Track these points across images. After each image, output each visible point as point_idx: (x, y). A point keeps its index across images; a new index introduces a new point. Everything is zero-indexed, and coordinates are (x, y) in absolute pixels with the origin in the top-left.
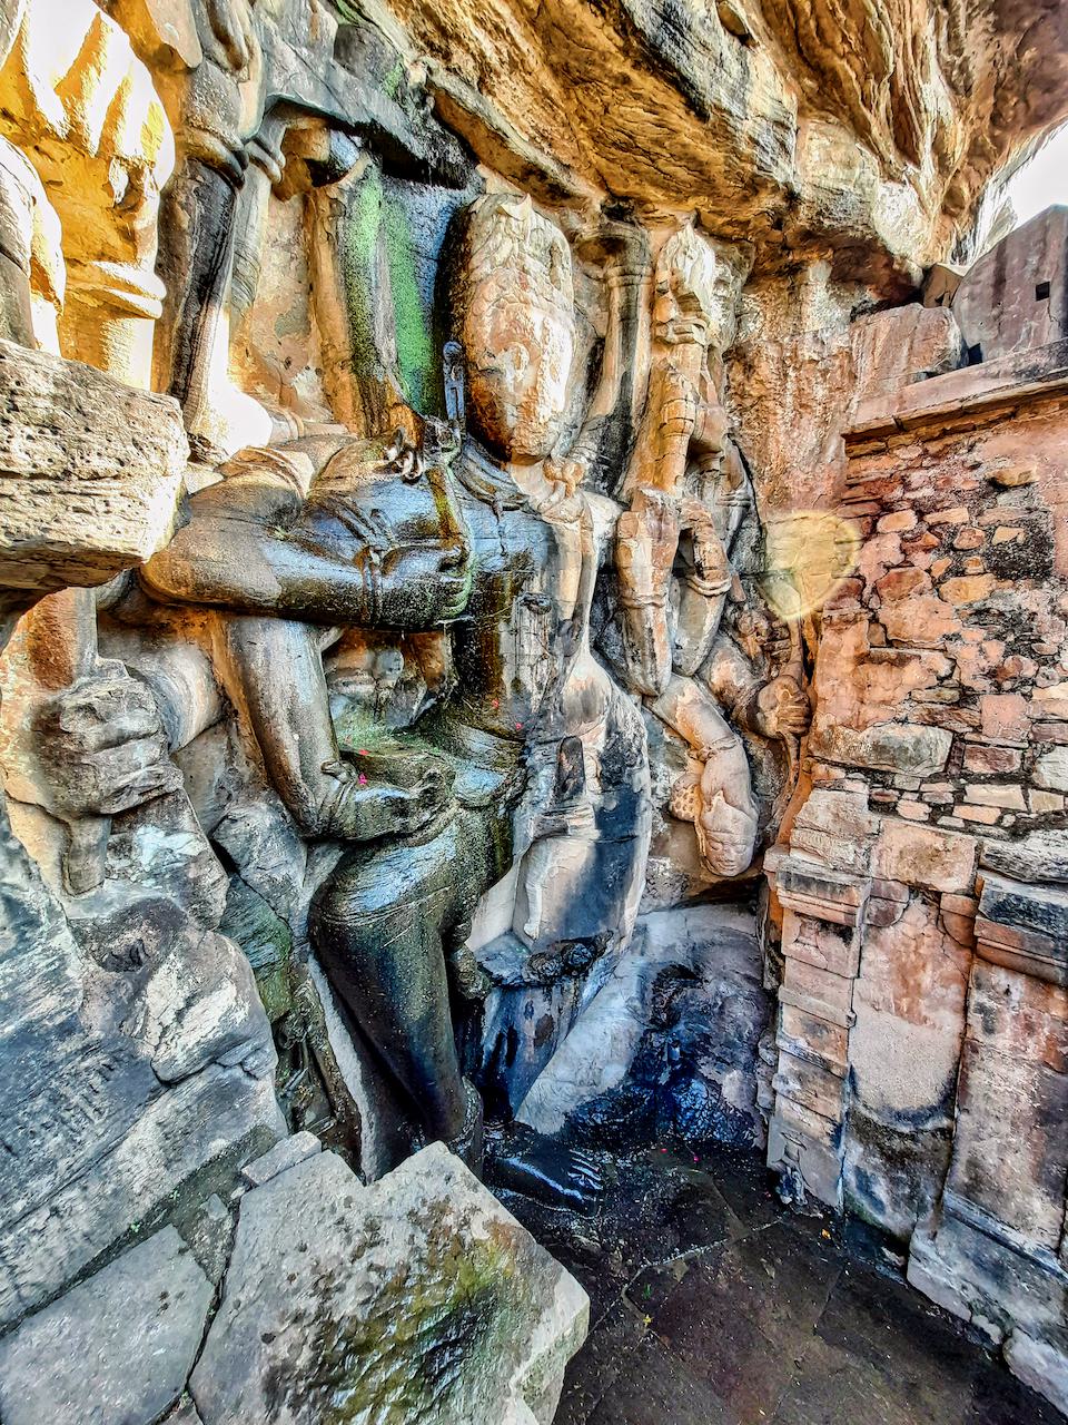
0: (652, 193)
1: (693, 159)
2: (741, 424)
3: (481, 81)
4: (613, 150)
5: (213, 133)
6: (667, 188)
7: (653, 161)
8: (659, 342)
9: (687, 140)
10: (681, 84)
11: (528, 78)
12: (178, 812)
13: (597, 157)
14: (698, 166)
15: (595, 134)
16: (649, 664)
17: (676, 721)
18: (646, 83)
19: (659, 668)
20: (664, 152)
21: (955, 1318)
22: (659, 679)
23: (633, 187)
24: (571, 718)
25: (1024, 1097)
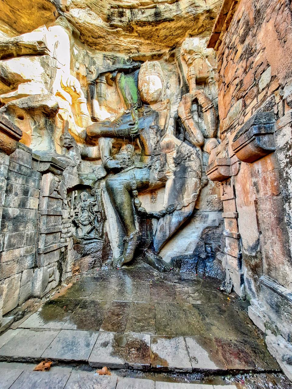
0: (177, 40)
1: (178, 28)
3: (138, 51)
6: (179, 37)
9: (174, 26)
10: (165, 20)
14: (182, 27)
18: (160, 26)
19: (195, 136)
20: (173, 32)
21: (259, 330)
22: (197, 139)
23: (173, 42)
24: (163, 149)
25: (272, 215)
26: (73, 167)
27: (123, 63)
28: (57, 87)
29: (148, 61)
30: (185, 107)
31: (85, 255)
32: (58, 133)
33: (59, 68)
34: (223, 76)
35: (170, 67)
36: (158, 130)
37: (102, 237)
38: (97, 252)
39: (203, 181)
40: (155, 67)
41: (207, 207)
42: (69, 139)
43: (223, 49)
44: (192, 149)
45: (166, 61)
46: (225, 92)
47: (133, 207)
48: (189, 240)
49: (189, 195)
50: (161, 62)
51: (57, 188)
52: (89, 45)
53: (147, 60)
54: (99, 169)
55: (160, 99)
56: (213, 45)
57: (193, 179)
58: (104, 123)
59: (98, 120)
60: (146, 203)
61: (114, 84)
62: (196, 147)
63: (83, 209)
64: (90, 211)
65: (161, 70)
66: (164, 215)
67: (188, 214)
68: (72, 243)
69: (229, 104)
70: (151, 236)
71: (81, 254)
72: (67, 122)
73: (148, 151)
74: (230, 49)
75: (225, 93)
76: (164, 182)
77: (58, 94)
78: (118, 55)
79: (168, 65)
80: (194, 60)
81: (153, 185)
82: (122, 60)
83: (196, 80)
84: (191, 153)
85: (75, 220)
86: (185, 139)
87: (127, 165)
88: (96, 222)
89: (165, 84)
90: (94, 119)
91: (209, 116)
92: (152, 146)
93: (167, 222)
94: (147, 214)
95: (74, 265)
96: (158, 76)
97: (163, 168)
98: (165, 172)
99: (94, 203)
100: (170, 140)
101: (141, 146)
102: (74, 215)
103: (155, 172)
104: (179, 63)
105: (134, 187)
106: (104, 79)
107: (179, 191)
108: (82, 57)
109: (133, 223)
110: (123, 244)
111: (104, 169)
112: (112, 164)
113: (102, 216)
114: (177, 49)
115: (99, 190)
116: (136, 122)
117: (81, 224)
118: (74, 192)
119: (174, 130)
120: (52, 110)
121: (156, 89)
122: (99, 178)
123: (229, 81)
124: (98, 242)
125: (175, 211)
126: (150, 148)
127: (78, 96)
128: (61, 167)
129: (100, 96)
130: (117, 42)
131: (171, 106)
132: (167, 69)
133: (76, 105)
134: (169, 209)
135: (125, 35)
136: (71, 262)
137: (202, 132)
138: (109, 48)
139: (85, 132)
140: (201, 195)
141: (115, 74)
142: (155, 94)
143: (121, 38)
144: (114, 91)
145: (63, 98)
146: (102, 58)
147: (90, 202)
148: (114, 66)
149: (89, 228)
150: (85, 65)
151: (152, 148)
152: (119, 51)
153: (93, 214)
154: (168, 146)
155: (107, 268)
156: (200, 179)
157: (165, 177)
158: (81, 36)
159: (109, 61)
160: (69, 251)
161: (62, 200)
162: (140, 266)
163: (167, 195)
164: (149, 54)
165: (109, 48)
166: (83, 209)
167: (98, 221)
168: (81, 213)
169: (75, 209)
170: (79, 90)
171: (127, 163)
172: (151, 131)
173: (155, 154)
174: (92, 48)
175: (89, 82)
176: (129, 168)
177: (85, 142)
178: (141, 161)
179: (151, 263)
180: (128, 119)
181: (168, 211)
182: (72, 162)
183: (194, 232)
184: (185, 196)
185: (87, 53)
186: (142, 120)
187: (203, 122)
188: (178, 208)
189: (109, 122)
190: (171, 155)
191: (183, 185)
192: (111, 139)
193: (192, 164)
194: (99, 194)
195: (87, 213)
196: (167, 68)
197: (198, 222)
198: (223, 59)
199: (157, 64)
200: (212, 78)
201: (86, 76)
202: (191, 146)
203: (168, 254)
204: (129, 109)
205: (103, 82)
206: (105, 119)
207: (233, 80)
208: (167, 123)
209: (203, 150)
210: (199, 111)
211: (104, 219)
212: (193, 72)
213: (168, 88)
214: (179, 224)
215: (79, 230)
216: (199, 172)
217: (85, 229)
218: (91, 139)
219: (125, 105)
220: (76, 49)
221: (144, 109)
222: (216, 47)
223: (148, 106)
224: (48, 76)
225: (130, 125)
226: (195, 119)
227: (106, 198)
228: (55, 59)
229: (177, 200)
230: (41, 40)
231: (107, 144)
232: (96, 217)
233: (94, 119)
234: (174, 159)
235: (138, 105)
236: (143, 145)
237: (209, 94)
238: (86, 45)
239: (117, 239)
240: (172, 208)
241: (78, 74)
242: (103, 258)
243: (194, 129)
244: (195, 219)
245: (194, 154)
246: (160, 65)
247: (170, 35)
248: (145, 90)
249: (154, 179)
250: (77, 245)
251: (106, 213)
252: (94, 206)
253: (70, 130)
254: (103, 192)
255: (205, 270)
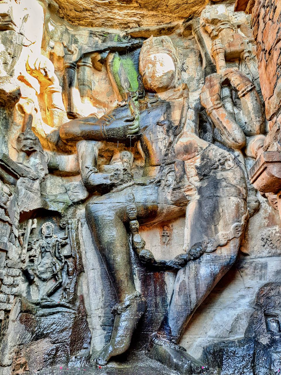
0: (194, 9)
4: (176, 10)
5: (67, 63)
7: (187, 3)
11: (147, 16)
12: (37, 155)
13: (175, 15)
15: (170, 12)
16: (226, 133)
19: (230, 132)
23: (189, 12)
24: (178, 154)
26: (34, 180)
27: (118, 41)
28: (19, 68)
29: (154, 36)
30: (211, 93)
31: (39, 337)
32: (15, 132)
33: (26, 46)
34: (261, 42)
35: (186, 43)
36: (170, 127)
37: (73, 302)
38: (62, 331)
39: (250, 204)
40: (164, 43)
41: (263, 249)
42: (31, 139)
43: (257, 10)
44: (226, 153)
45: (180, 35)
46: (267, 61)
47: (132, 250)
48: (234, 312)
49: (226, 225)
50: (173, 37)
51: (5, 204)
52: (70, 20)
53: (152, 36)
54: (75, 187)
55: (172, 85)
56: (243, 7)
57: (233, 198)
58: (86, 120)
59: (78, 116)
60: (154, 244)
61: (103, 69)
62: (233, 151)
63: (43, 251)
64: (55, 256)
65: (172, 46)
66: (184, 263)
67: (228, 260)
68: (19, 308)
69: (274, 76)
70: (163, 306)
71: (33, 334)
72: (31, 117)
73: (155, 160)
74: (267, 7)
75: (267, 63)
76: (183, 208)
77: (21, 79)
78: (110, 31)
79: (183, 40)
80: (220, 30)
81: (165, 211)
82: (116, 37)
83: (226, 57)
84: (225, 158)
85: (29, 268)
86: (214, 140)
87: (122, 181)
88: (64, 275)
89: (179, 65)
90: (71, 115)
91: (249, 102)
92: (161, 151)
93: (192, 275)
94: (155, 262)
95: (18, 353)
96: (169, 54)
97: (180, 184)
98: (183, 190)
99: (64, 241)
100: (189, 141)
101: (144, 152)
102: (27, 260)
103: (166, 190)
104: (198, 37)
105: (133, 214)
106: (89, 61)
107: (209, 217)
108: (59, 34)
109: (131, 278)
110: (111, 324)
111: (84, 187)
112: (97, 179)
113: (76, 265)
114: (194, 20)
115: (74, 221)
116: (136, 117)
117: (38, 276)
118: (31, 221)
119: (195, 126)
120: (10, 97)
121: (166, 72)
122: (76, 200)
123: (270, 47)
124: (66, 312)
125: (205, 254)
126: (158, 154)
127: (50, 82)
128: (15, 171)
129: (82, 84)
130: (109, 15)
131: (190, 93)
132: (181, 46)
133: (46, 96)
134: (193, 251)
135: (120, 6)
136: (13, 345)
137: (241, 127)
138: (97, 23)
139: (56, 133)
140: (250, 228)
141: (105, 55)
142: (165, 77)
143: (116, 10)
144: (104, 77)
145: (28, 84)
146: (88, 35)
147: (56, 239)
148: (105, 44)
149: (51, 285)
150: (62, 43)
151: (161, 154)
152: (112, 26)
153: (61, 261)
154: (188, 150)
155: (78, 365)
156: (245, 200)
157: (184, 197)
158: (60, 10)
159: (97, 39)
160: (10, 322)
161: (11, 225)
162: (141, 364)
163: (189, 229)
164: (155, 28)
165: (97, 22)
166: (43, 251)
167: (68, 274)
168: (40, 257)
169: (29, 250)
170: (51, 74)
171: (121, 177)
172: (158, 129)
173: (167, 162)
174: (74, 23)
175: (67, 64)
176: (125, 185)
177: (55, 148)
178: (145, 175)
179: (163, 359)
180: (124, 114)
181: (192, 255)
182: (33, 172)
183: (243, 297)
184: (220, 227)
185: (67, 30)
186: (145, 114)
187: (241, 112)
188: (209, 249)
189: (94, 119)
190: (192, 163)
191: (215, 209)
192: (97, 142)
193: (229, 175)
194: (73, 226)
195: (51, 258)
196: (182, 44)
197: (249, 277)
198: (258, 22)
199: (166, 40)
200: (249, 52)
201: (63, 57)
202: (225, 149)
203: (197, 342)
204: (126, 100)
205: (88, 65)
206: (89, 115)
207: (276, 44)
208: (184, 115)
209: (245, 155)
210: (234, 97)
211: (79, 270)
212: (219, 46)
213: (183, 70)
214: (214, 280)
215: (33, 288)
216: (241, 189)
217: (44, 287)
218: (65, 144)
219: (120, 97)
220: (52, 25)
221: (149, 99)
222: (247, 10)
223: (155, 94)
224: (9, 56)
225: (127, 121)
226: (228, 109)
227: (85, 234)
228: (22, 34)
229: (207, 235)
230: (5, 13)
231: (90, 150)
232: (66, 266)
233: (71, 115)
234: (197, 168)
235: (139, 94)
236: (146, 150)
237: (247, 73)
238: (65, 20)
239: (100, 310)
240: (198, 249)
241: (51, 55)
242: (73, 343)
243: (228, 122)
244: (242, 272)
245: (231, 160)
246: (171, 40)
247: (183, 4)
248: (149, 73)
249: (166, 202)
250: (26, 313)
251: (83, 260)
252: (63, 246)
253: (34, 128)
254: (80, 223)
255: (270, 370)
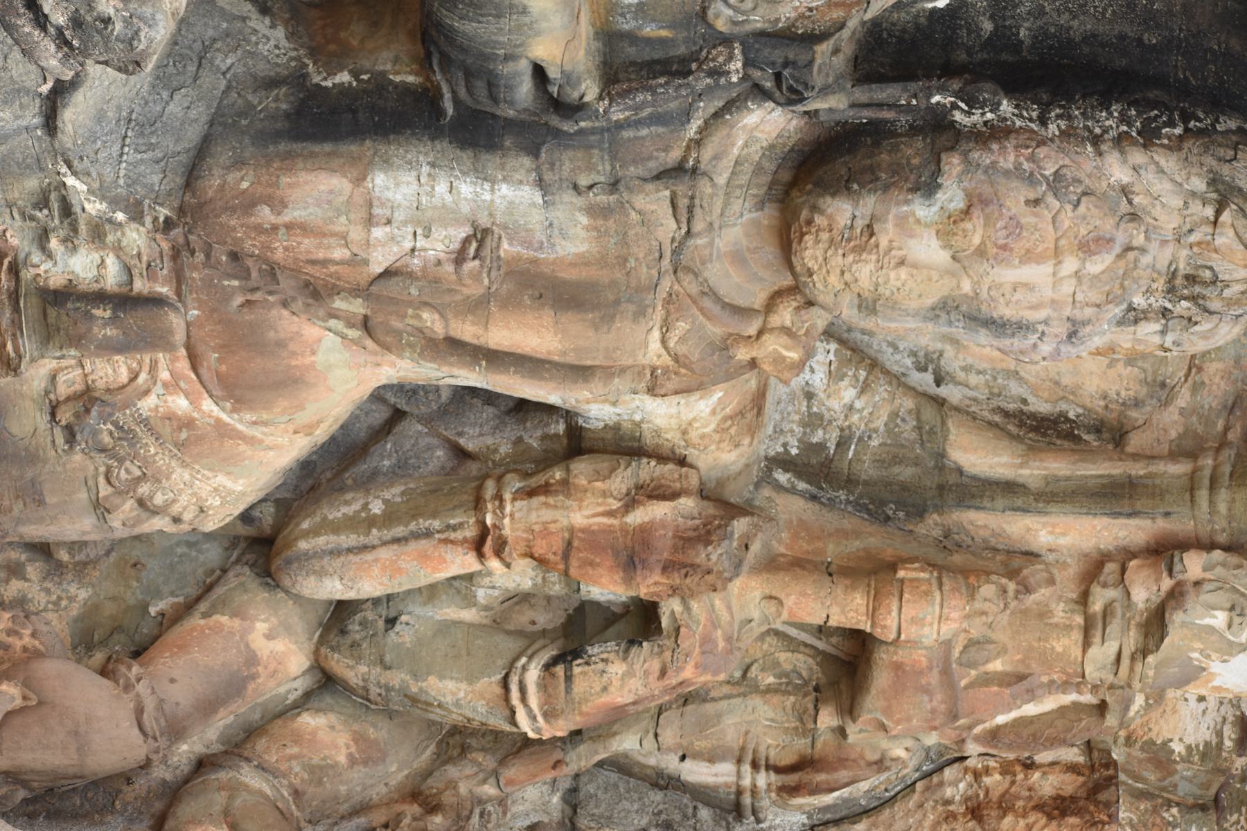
2: (948, 802)
8: (1094, 569)
17: (206, 615)
